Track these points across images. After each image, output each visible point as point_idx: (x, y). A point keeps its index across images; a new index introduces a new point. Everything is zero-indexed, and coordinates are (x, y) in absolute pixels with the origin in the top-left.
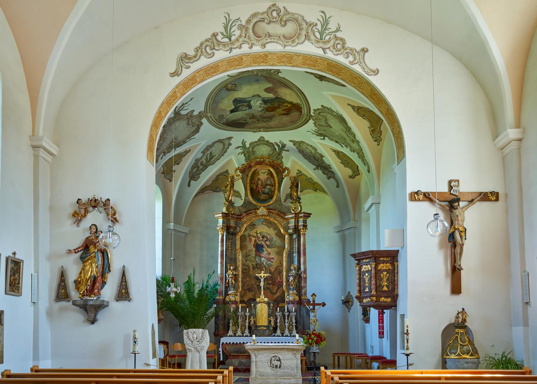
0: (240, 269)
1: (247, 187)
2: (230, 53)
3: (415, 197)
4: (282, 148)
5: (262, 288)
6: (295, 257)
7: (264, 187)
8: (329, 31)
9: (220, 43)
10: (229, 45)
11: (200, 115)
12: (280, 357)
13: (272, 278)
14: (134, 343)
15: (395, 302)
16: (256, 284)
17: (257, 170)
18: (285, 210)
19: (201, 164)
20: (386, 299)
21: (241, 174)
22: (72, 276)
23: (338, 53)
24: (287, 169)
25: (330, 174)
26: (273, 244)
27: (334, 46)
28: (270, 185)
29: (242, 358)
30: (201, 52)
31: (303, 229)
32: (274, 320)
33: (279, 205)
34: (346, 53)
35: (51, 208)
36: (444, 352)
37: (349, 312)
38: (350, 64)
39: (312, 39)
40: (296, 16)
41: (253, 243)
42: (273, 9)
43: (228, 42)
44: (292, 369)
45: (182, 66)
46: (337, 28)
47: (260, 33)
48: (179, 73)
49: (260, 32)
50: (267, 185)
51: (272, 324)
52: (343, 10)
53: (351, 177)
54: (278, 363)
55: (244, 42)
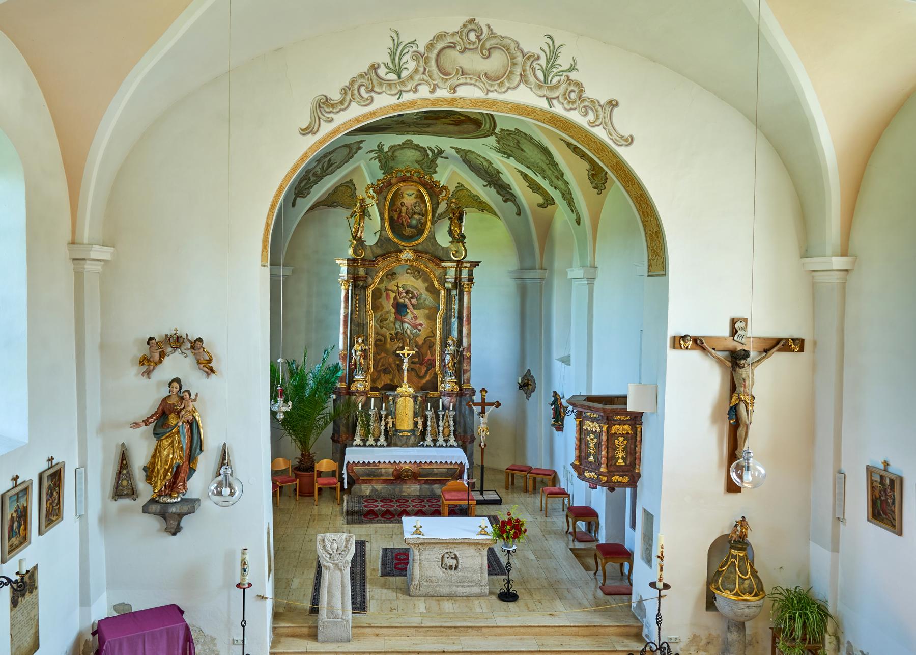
0: (372, 340)
1: (384, 216)
2: (398, 99)
3: (680, 344)
4: (438, 155)
5: (405, 372)
6: (454, 324)
7: (410, 216)
8: (558, 70)
9: (384, 82)
10: (398, 86)
12: (457, 553)
13: (419, 354)
14: (243, 572)
15: (634, 483)
16: (395, 363)
17: (400, 190)
18: (440, 254)
19: (314, 175)
20: (621, 478)
21: (375, 195)
22: (140, 458)
23: (571, 106)
24: (445, 189)
25: (508, 197)
26: (422, 303)
27: (565, 94)
28: (419, 214)
29: (376, 483)
30: (352, 95)
31: (468, 284)
32: (422, 421)
33: (432, 245)
34: (584, 107)
35: (103, 347)
36: (713, 579)
37: (528, 400)
38: (590, 126)
39: (531, 82)
40: (506, 42)
41: (392, 301)
42: (470, 27)
43: (396, 80)
44: (474, 572)
45: (319, 118)
46: (571, 64)
47: (448, 67)
48: (315, 129)
49: (448, 66)
50: (415, 213)
51: (419, 427)
52: (582, 35)
53: (540, 206)
54: (453, 562)
55: (422, 82)
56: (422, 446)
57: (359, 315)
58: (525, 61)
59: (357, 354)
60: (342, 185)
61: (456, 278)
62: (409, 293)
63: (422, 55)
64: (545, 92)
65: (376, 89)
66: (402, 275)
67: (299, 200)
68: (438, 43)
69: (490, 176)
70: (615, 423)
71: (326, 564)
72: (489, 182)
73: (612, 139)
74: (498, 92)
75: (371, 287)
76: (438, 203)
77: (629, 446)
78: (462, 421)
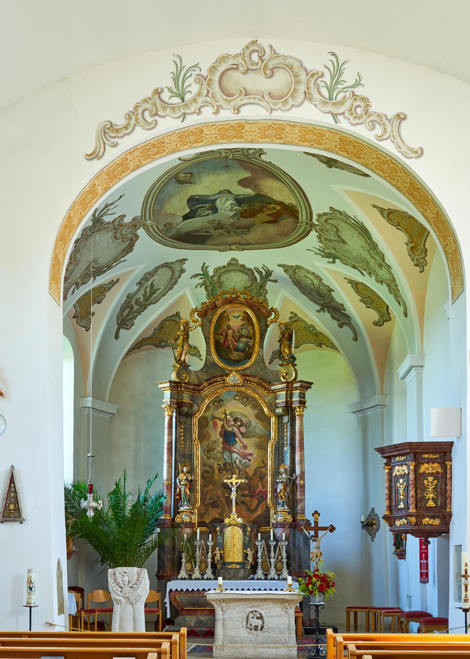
0: (199, 471)
4: (266, 278)
6: (287, 453)
7: (237, 339)
11: (135, 222)
12: (262, 612)
14: (29, 590)
17: (226, 312)
21: (199, 319)
23: (357, 121)
25: (343, 320)
26: (251, 432)
28: (246, 337)
29: (201, 615)
30: (136, 120)
31: (299, 407)
33: (261, 369)
34: (371, 121)
37: (373, 541)
38: (377, 139)
40: (289, 61)
41: (219, 429)
42: (252, 48)
43: (179, 103)
44: (281, 633)
45: (104, 143)
48: (101, 154)
49: (231, 87)
50: (242, 336)
51: (249, 559)
53: (376, 324)
54: (259, 622)
55: (206, 104)
57: (185, 445)
58: (308, 79)
59: (182, 483)
60: (168, 319)
61: (286, 402)
62: (238, 421)
63: (205, 78)
64: (330, 108)
65: (160, 113)
66: (230, 402)
67: (122, 331)
68: (220, 65)
69: (322, 297)
70: (423, 461)
71: (117, 598)
72: (321, 305)
73: (401, 152)
74: (282, 110)
75: (197, 415)
76: (267, 326)
77: (439, 487)
78: (297, 555)
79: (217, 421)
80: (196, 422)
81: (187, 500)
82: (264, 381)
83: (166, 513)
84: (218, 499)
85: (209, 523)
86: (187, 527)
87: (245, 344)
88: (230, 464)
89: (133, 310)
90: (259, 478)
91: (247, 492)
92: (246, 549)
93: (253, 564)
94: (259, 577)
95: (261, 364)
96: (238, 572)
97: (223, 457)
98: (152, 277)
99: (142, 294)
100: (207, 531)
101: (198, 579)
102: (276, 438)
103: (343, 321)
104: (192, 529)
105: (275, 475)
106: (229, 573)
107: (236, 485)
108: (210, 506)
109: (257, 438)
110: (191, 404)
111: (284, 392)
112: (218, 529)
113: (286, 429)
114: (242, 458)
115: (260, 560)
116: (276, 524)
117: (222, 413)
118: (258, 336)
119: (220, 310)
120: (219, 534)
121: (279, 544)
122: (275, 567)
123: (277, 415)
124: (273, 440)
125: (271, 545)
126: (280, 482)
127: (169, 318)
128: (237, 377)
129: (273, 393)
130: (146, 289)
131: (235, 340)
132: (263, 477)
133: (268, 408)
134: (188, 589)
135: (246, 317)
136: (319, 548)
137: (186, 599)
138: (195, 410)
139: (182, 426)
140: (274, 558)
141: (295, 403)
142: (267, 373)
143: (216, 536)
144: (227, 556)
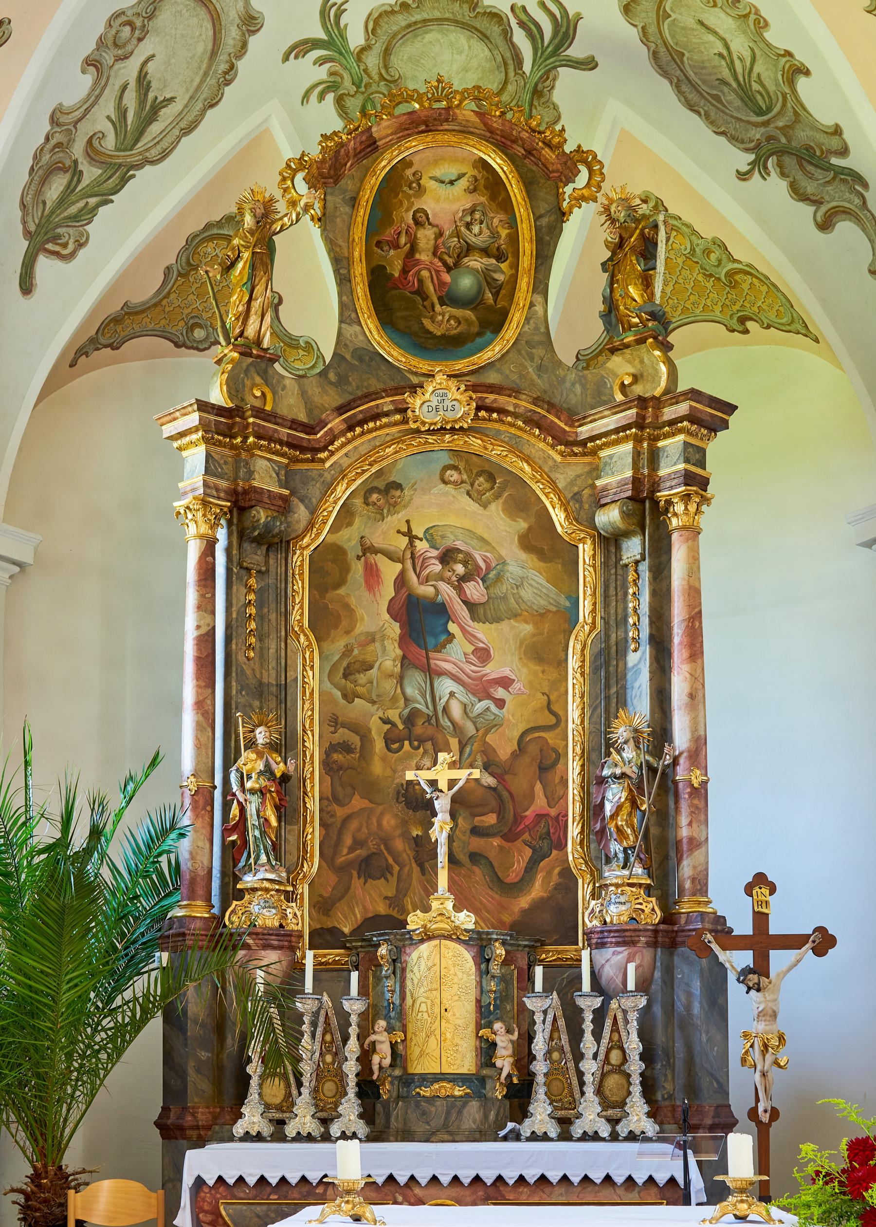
0: (313, 746)
4: (555, 52)
6: (638, 672)
7: (450, 261)
13: (500, 797)
16: (406, 835)
25: (837, 195)
26: (505, 598)
28: (485, 252)
33: (540, 368)
41: (388, 591)
50: (469, 249)
51: (499, 1063)
56: (516, 1136)
59: (249, 785)
61: (636, 481)
62: (456, 561)
67: (44, 265)
69: (760, 112)
72: (756, 148)
75: (306, 540)
76: (562, 215)
78: (679, 1046)
79: (382, 561)
80: (302, 566)
81: (270, 848)
82: (551, 407)
83: (192, 896)
84: (387, 848)
85: (353, 933)
86: (267, 946)
87: (482, 278)
88: (429, 719)
89: (79, 181)
90: (535, 769)
91: (491, 819)
92: (489, 1025)
93: (515, 1081)
94: (635, 1127)
95: (539, 352)
96: (460, 1112)
97: (403, 693)
98: (140, 40)
99: (108, 118)
100: (346, 963)
101: (310, 1138)
102: (598, 619)
103: (834, 204)
104: (288, 953)
105: (594, 756)
106: (424, 1113)
107: (450, 789)
108: (355, 874)
109: (527, 622)
110: (285, 499)
111: (628, 447)
112: (383, 950)
113: (636, 584)
114: (474, 694)
115: (540, 1067)
116: (602, 932)
117: (399, 532)
118: (527, 248)
119: (387, 156)
120: (386, 970)
121: (614, 1004)
122: (599, 1091)
123: (600, 534)
124: (587, 628)
125: (582, 1010)
126: (615, 776)
127: (215, 231)
128: (453, 394)
129: (584, 454)
130: (121, 97)
131: (445, 264)
132: (549, 762)
133: (566, 510)
134: (266, 1175)
135: (482, 182)
136: (774, 1015)
137: (258, 1216)
138: (298, 522)
139: (252, 581)
140: (595, 1056)
141: (668, 484)
142: (563, 381)
143: (378, 979)
144: (416, 1051)
